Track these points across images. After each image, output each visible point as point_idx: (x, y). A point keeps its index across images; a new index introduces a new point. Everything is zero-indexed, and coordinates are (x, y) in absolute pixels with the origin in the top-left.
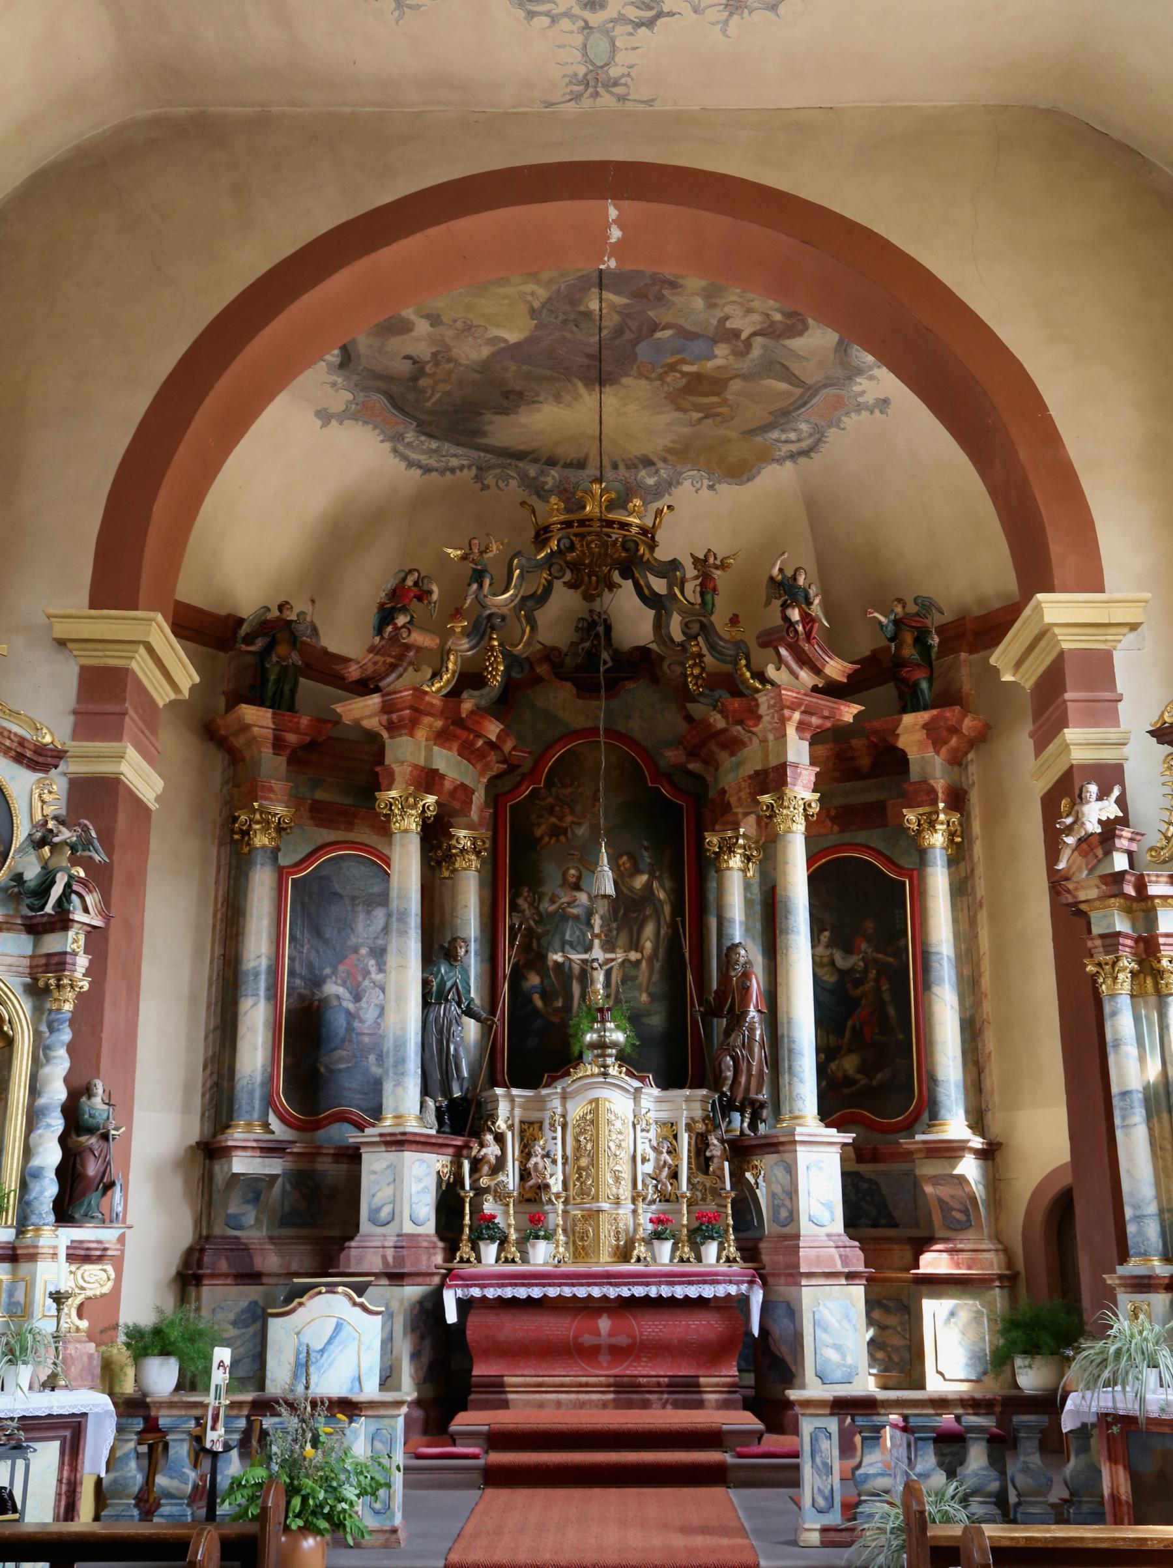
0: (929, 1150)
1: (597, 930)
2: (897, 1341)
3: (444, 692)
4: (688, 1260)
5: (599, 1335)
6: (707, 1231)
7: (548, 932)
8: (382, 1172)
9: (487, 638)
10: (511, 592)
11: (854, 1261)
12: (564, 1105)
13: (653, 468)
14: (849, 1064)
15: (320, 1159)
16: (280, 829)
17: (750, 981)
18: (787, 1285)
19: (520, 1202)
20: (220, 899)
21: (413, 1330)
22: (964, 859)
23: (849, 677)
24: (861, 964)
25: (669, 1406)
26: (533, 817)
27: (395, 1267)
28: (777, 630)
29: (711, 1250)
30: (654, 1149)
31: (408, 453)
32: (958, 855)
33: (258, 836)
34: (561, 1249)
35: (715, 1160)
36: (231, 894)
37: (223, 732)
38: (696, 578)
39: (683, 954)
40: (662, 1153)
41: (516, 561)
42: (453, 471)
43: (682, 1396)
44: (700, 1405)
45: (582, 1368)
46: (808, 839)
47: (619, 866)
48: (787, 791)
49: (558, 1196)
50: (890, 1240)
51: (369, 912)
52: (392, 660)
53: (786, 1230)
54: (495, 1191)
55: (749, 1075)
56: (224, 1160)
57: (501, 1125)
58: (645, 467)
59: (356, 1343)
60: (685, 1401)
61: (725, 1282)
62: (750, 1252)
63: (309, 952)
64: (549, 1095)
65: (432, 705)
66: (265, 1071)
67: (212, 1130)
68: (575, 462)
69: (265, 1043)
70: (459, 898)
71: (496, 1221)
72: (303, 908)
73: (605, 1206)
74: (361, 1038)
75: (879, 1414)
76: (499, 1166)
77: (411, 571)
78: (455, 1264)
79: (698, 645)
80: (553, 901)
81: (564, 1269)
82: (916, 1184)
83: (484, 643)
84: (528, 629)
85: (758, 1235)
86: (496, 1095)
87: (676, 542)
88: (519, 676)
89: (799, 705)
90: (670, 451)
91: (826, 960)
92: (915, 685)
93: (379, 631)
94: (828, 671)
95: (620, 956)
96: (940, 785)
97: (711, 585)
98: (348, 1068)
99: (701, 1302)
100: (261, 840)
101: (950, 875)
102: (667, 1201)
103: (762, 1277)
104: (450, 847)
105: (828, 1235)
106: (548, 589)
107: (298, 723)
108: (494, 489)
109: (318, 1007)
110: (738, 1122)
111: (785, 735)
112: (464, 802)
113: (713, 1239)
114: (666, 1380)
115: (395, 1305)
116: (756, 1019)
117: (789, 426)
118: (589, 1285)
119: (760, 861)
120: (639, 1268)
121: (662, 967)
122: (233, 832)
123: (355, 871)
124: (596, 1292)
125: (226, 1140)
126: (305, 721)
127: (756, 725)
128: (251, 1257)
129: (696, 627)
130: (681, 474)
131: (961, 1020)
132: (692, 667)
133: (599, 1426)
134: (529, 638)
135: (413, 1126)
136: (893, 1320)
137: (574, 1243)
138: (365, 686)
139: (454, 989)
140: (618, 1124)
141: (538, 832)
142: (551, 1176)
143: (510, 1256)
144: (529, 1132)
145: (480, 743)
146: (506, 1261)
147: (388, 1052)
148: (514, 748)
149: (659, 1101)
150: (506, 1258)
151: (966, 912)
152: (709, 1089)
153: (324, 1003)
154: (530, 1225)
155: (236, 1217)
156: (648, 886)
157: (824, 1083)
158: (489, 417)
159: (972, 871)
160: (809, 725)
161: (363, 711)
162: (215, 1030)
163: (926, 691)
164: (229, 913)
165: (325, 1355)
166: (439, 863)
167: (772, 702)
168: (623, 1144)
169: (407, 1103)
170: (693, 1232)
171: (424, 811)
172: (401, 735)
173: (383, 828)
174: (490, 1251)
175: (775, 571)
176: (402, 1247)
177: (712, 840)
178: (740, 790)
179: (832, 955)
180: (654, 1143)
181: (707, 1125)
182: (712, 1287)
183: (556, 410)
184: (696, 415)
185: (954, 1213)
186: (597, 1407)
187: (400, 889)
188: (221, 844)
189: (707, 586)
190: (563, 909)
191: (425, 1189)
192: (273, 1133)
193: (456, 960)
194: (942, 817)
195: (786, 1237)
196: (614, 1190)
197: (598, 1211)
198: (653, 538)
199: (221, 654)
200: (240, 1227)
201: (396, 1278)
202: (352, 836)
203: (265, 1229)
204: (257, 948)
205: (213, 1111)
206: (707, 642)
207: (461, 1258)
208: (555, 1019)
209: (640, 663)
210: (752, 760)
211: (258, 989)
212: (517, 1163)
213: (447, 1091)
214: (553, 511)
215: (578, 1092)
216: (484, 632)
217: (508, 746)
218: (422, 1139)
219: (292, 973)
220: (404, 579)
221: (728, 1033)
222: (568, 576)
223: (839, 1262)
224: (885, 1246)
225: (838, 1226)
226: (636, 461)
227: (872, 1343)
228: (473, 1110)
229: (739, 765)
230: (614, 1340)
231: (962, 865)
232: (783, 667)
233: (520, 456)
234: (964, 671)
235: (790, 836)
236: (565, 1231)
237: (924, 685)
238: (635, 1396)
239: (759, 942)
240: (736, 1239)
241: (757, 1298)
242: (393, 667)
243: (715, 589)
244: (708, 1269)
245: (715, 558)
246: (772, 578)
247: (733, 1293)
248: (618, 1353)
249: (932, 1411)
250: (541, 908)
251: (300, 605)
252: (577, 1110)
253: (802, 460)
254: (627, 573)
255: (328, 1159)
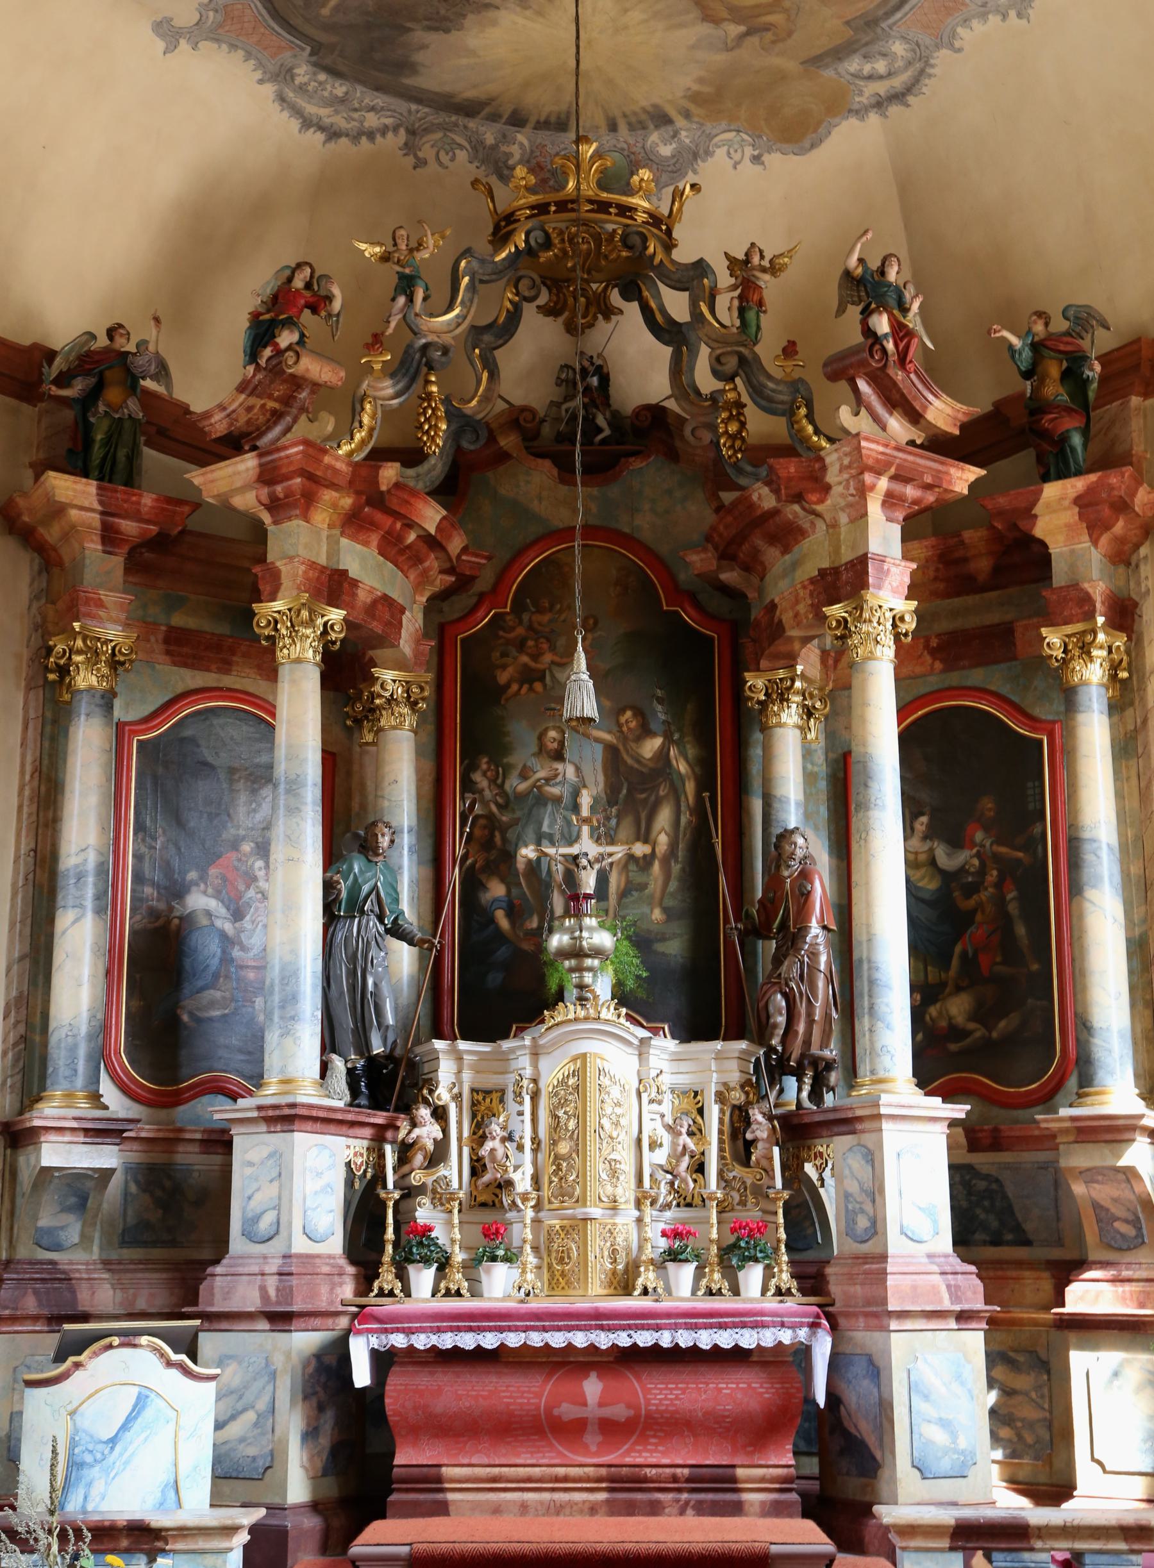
0: (1080, 1130)
1: (585, 812)
2: (1029, 1412)
3: (358, 458)
4: (719, 1292)
5: (585, 1404)
6: (748, 1249)
7: (516, 822)
8: (262, 1163)
9: (420, 381)
10: (457, 311)
11: (969, 1294)
12: (535, 1065)
13: (670, 128)
14: (958, 1008)
15: (181, 1148)
16: (115, 664)
17: (812, 884)
18: (868, 1328)
19: (471, 1207)
20: (29, 769)
21: (306, 1398)
22: (1132, 704)
23: (963, 427)
24: (976, 862)
25: (690, 1511)
26: (496, 655)
27: (278, 1303)
28: (854, 351)
29: (752, 1277)
30: (669, 1128)
31: (301, 103)
32: (1124, 695)
33: (82, 674)
34: (530, 1276)
35: (760, 1145)
36: (46, 762)
37: (26, 519)
38: (734, 288)
39: (712, 847)
40: (680, 1134)
41: (463, 264)
42: (371, 135)
43: (710, 1496)
44: (736, 1509)
45: (560, 1453)
46: (900, 680)
47: (620, 726)
48: (868, 597)
49: (525, 1198)
50: (1020, 1264)
51: (254, 792)
52: (276, 405)
53: (865, 1248)
54: (434, 1191)
55: (810, 1022)
56: (31, 1147)
57: (443, 1094)
58: (657, 127)
59: (171, 1427)
60: (714, 1503)
61: (774, 1325)
62: (812, 1281)
63: (164, 847)
64: (512, 1050)
65: (336, 471)
66: (93, 1017)
67: (18, 1105)
68: (553, 119)
69: (93, 976)
70: (387, 769)
71: (433, 1234)
72: (155, 784)
73: (595, 1212)
74: (242, 973)
75: (1032, 1550)
76: (439, 1155)
77: (299, 266)
78: (371, 1299)
79: (735, 389)
80: (524, 777)
81: (534, 1305)
82: (1058, 1181)
83: (417, 386)
84: (485, 375)
85: (823, 1256)
86: (435, 1051)
87: (706, 234)
88: (472, 447)
89: (888, 465)
90: (695, 98)
91: (922, 857)
92: (1064, 439)
93: (253, 356)
94: (930, 416)
95: (619, 851)
96: (1098, 590)
97: (756, 297)
98: (225, 1016)
99: (738, 1355)
100: (85, 679)
101: (1111, 727)
102: (689, 1205)
103: (830, 1317)
104: (373, 696)
105: (930, 1256)
106: (515, 316)
107: (139, 503)
108: (433, 166)
109: (179, 928)
110: (793, 1092)
111: (866, 514)
112: (388, 624)
113: (756, 1260)
114: (686, 1471)
115: (278, 1361)
116: (820, 940)
117: (876, 48)
118: (569, 1329)
119: (826, 717)
120: (646, 1303)
121: (683, 870)
122: (47, 669)
123: (234, 731)
124: (580, 1340)
125: (31, 1119)
126: (148, 501)
127: (821, 501)
128: (73, 1292)
129: (732, 363)
130: (711, 137)
131: (1129, 941)
132: (726, 422)
133: (580, 1547)
134: (487, 389)
135: (309, 1094)
136: (1023, 1382)
137: (550, 1266)
138: (234, 444)
139: (373, 896)
140: (615, 1092)
141: (503, 677)
142: (516, 1168)
143: (453, 1287)
144: (484, 1104)
145: (412, 537)
146: (448, 1293)
147: (272, 985)
148: (465, 550)
149: (677, 1059)
150: (448, 1290)
151: (1134, 781)
152: (751, 1041)
153: (187, 920)
154: (484, 1241)
155: (50, 1231)
156: (662, 755)
157: (920, 1036)
158: (420, 35)
159: (1145, 721)
160: (902, 499)
161: (232, 481)
162: (22, 959)
163: (1079, 449)
164: (43, 788)
165: (118, 1449)
166: (358, 722)
167: (846, 461)
168: (623, 1121)
169: (297, 1059)
170: (726, 1252)
171: (325, 632)
172: (289, 519)
173: (268, 666)
174: (423, 1278)
175: (853, 261)
176: (290, 1274)
177: (756, 683)
178: (797, 602)
179: (931, 850)
180: (669, 1120)
181: (747, 1094)
182: (754, 1332)
183: (520, 21)
184: (735, 30)
185: (1117, 1224)
186: (581, 1512)
187: (289, 747)
188: (29, 688)
189: (749, 297)
190: (539, 788)
191: (328, 1188)
192: (106, 1108)
193: (378, 855)
194: (1101, 637)
195: (866, 1258)
196: (609, 1189)
197: (585, 1219)
198: (669, 232)
199: (25, 407)
200: (58, 1248)
201: (281, 1319)
202: (228, 681)
203: (96, 1249)
204: (83, 836)
205: (19, 1077)
206: (749, 383)
207: (381, 1289)
208: (527, 946)
209: (652, 428)
210: (816, 554)
211: (82, 897)
212: (466, 1151)
213: (363, 1046)
214: (517, 192)
215: (556, 1044)
216: (417, 372)
217: (455, 545)
218: (322, 1114)
219: (138, 878)
220: (290, 280)
221: (778, 961)
222: (544, 298)
223: (946, 1296)
224: (1013, 1274)
225: (944, 1241)
226: (644, 117)
227: (993, 1412)
228: (402, 1073)
229: (795, 565)
230: (610, 1412)
231: (1129, 712)
232: (863, 411)
233: (469, 109)
234: (1136, 424)
235: (873, 666)
236: (536, 1249)
237: (1077, 440)
238: (639, 1496)
239: (824, 833)
240: (791, 1262)
241: (822, 1347)
242: (277, 416)
243: (760, 303)
244: (748, 1306)
245: (762, 257)
246: (847, 274)
247: (787, 1342)
248: (614, 1430)
249: (1123, 1546)
250: (507, 787)
251: (141, 331)
252: (553, 1070)
253: (894, 110)
254: (631, 292)
255: (195, 1148)
